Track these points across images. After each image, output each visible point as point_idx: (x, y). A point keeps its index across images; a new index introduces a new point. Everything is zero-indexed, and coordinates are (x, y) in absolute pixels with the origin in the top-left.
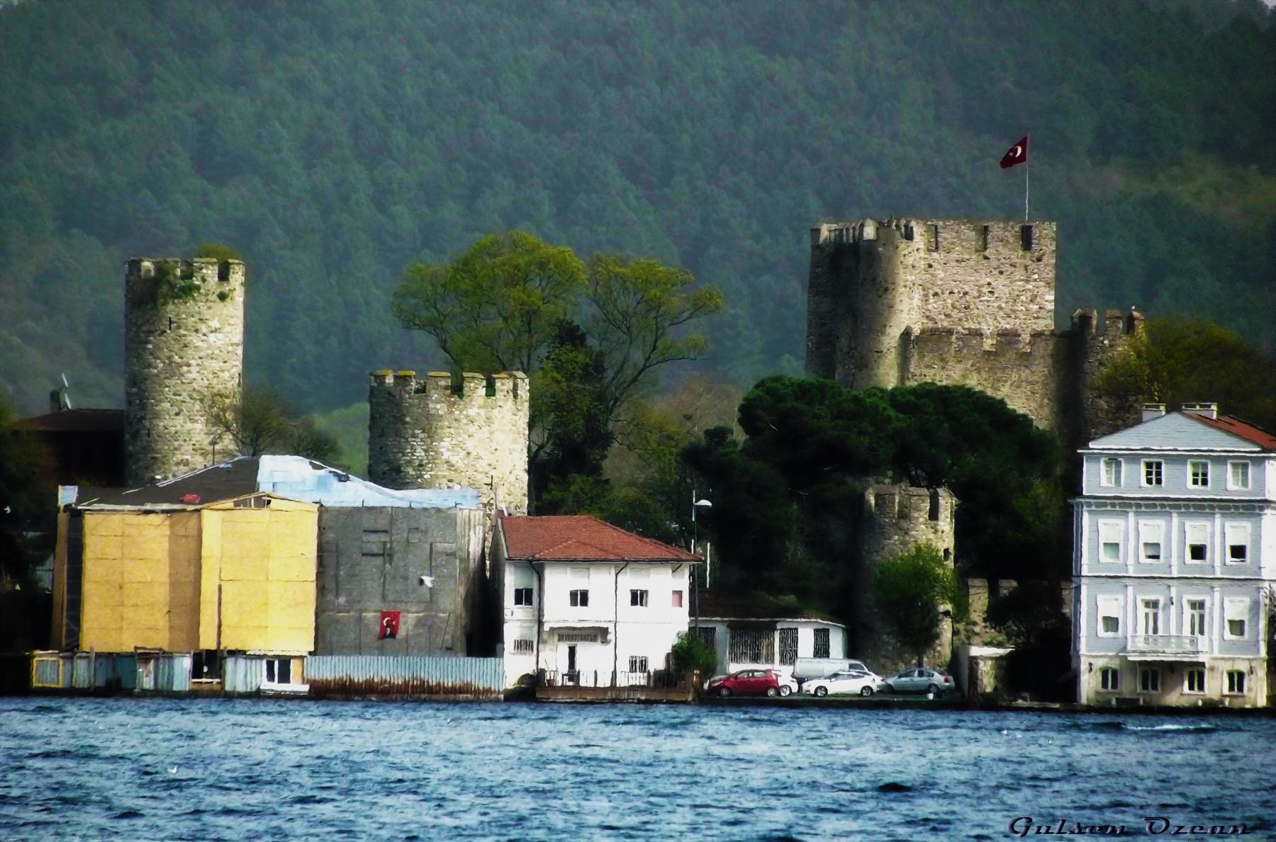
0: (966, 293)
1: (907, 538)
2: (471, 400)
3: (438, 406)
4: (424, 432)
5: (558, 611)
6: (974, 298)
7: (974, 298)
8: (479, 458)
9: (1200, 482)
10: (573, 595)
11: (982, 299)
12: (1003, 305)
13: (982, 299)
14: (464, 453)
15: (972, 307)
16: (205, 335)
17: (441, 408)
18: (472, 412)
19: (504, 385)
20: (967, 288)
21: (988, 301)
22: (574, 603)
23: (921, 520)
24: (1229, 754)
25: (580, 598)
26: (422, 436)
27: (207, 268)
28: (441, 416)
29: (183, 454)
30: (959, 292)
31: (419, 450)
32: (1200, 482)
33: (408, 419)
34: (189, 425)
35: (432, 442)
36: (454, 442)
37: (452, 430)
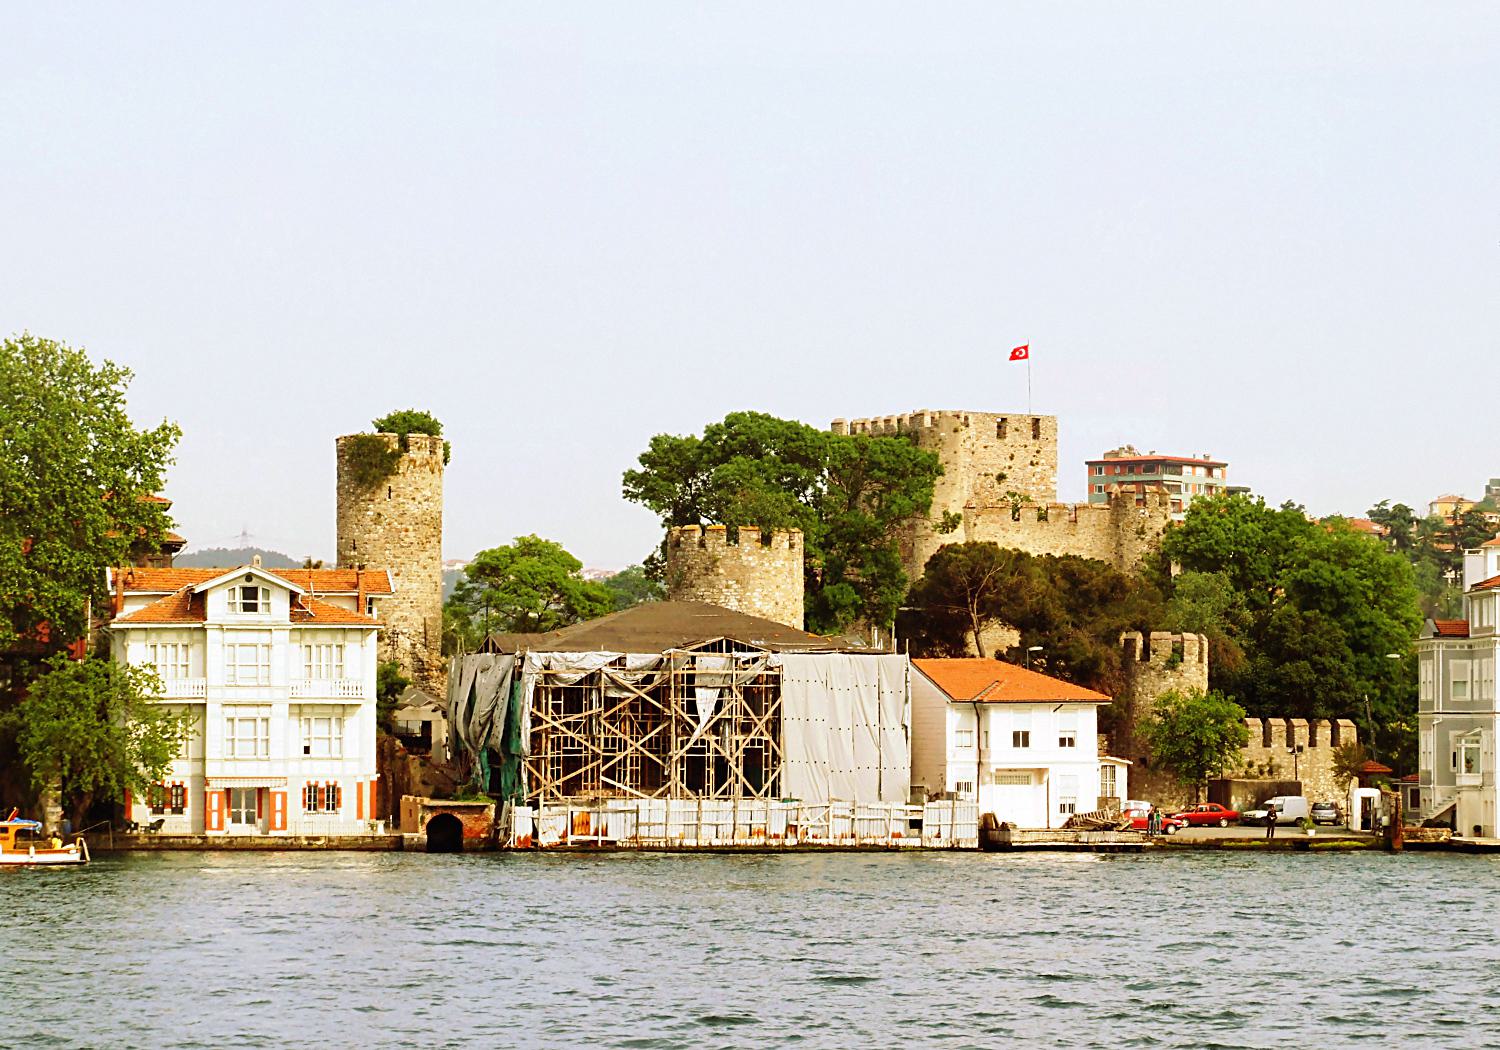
1: (1182, 680)
3: (750, 558)
4: (737, 582)
5: (1002, 753)
8: (785, 607)
9: (676, 775)
10: (1016, 735)
14: (773, 603)
17: (752, 561)
18: (779, 564)
19: (780, 539)
22: (1016, 744)
23: (1193, 663)
24: (1127, 983)
25: (1021, 739)
26: (735, 586)
29: (951, 523)
31: (733, 599)
32: (676, 775)
33: (721, 571)
34: (407, 585)
35: (745, 592)
36: (765, 593)
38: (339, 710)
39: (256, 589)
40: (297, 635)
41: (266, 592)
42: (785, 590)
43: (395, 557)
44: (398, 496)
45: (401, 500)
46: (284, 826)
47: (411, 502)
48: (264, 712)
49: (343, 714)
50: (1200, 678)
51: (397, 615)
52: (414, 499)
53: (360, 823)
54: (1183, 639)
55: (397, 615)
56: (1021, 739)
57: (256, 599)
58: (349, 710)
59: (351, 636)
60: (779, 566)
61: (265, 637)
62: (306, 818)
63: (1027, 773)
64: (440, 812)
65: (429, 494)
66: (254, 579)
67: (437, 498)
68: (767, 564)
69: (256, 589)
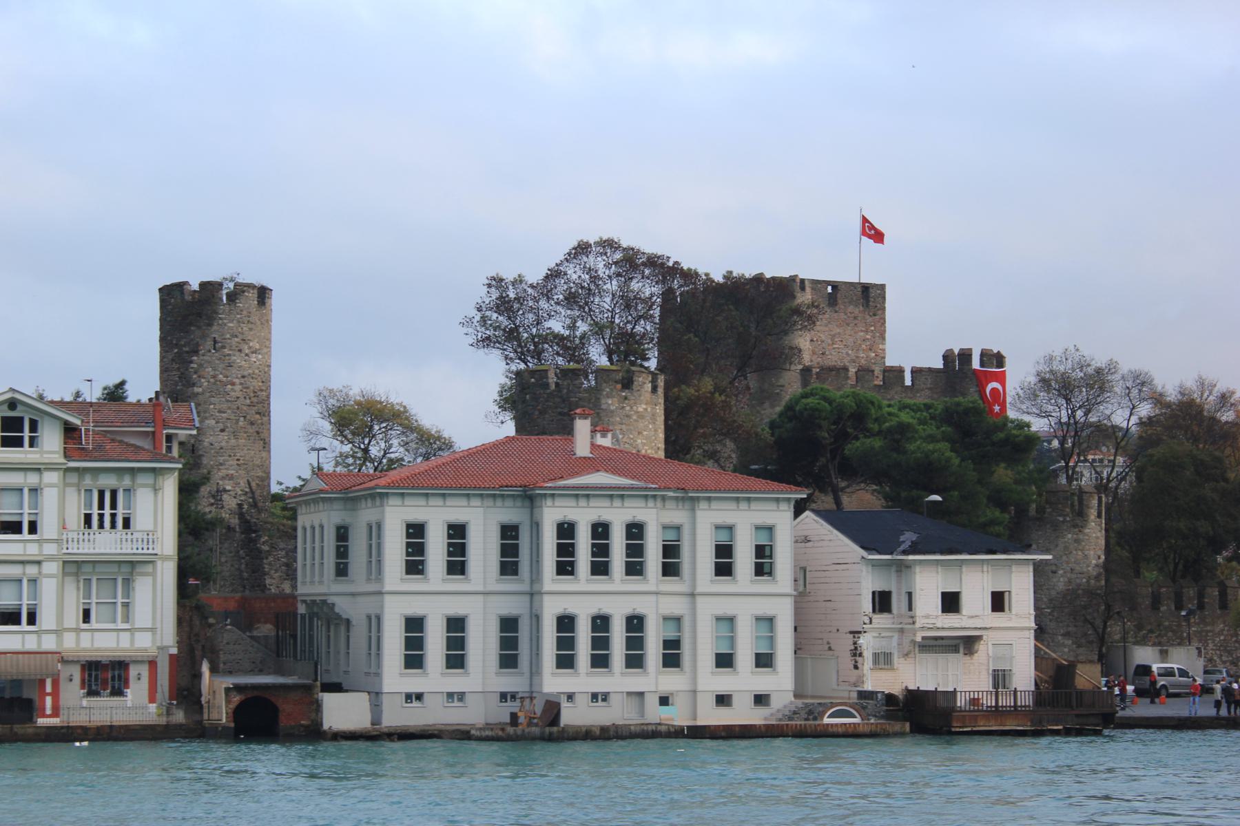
0: (823, 341)
2: (640, 396)
6: (829, 345)
7: (829, 345)
11: (835, 346)
12: (850, 352)
13: (835, 346)
15: (827, 353)
16: (247, 355)
20: (823, 338)
21: (838, 348)
27: (249, 292)
28: (612, 412)
30: (817, 340)
37: (624, 427)
38: (126, 569)
39: (21, 419)
40: (73, 478)
41: (34, 426)
42: (647, 438)
43: (220, 412)
44: (223, 347)
45: (226, 351)
46: (56, 713)
47: (237, 353)
48: (32, 570)
49: (131, 573)
50: (1099, 534)
51: (223, 473)
52: (240, 351)
53: (153, 707)
54: (657, 586)
55: (223, 473)
56: (951, 602)
57: (22, 432)
58: (139, 569)
59: (142, 479)
60: (640, 409)
61: (33, 479)
62: (85, 703)
63: (957, 641)
64: (250, 694)
65: (257, 346)
66: (20, 407)
67: (265, 350)
68: (628, 408)
69: (21, 419)
